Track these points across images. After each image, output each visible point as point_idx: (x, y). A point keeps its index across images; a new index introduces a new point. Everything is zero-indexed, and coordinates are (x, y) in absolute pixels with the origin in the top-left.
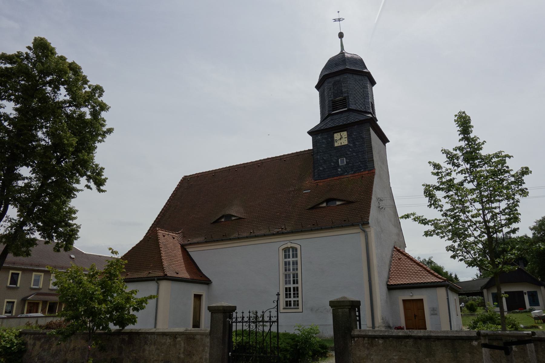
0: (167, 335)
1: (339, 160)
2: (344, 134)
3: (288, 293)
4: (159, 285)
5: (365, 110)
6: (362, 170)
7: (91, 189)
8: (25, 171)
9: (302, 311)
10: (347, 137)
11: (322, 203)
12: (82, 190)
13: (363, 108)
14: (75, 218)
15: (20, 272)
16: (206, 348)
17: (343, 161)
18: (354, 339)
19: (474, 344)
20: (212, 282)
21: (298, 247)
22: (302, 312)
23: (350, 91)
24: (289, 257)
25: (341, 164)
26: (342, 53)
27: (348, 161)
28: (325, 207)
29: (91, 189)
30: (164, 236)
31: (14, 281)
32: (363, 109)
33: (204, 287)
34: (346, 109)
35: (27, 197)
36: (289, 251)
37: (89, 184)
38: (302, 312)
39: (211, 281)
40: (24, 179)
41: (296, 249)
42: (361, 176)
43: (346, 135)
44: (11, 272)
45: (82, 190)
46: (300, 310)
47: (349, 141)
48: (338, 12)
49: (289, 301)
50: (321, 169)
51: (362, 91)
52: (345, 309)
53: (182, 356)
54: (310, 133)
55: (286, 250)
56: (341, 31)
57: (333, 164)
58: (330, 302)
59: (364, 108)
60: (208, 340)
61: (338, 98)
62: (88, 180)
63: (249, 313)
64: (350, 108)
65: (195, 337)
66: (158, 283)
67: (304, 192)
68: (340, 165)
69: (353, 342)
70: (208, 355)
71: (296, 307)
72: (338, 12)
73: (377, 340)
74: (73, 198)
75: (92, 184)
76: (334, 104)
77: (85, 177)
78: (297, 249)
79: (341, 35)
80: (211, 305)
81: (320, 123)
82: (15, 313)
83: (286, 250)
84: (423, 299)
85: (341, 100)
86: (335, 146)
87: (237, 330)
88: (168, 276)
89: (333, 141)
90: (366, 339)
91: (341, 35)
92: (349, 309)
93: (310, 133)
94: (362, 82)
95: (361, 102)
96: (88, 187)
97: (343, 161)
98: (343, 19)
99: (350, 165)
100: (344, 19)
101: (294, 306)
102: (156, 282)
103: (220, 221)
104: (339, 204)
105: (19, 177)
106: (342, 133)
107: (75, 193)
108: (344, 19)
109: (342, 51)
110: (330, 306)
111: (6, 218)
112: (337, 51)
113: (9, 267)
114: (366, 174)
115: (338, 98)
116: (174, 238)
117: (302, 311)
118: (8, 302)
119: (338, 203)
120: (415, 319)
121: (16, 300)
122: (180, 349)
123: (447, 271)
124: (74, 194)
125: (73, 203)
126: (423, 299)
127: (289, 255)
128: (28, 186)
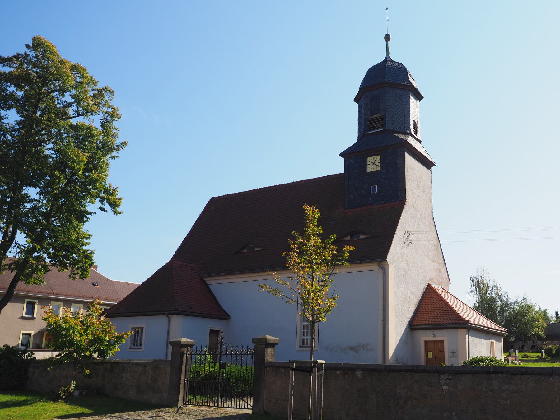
0: (139, 365)
1: (371, 187)
2: (378, 158)
3: (305, 330)
4: (170, 320)
5: (404, 131)
6: (394, 200)
7: (106, 211)
8: (32, 192)
9: (317, 350)
10: (368, 166)
11: (346, 236)
12: (95, 213)
13: (402, 128)
14: (88, 243)
15: (37, 301)
16: (167, 375)
17: (374, 189)
18: (267, 369)
19: (338, 373)
20: (231, 318)
22: (318, 351)
23: (387, 109)
25: (372, 192)
26: (388, 59)
27: (380, 189)
28: (348, 240)
29: (106, 211)
30: (181, 267)
31: (31, 311)
32: (402, 130)
33: (223, 322)
34: (382, 129)
35: (27, 230)
37: (103, 206)
38: (318, 351)
39: (229, 316)
40: (31, 201)
42: (391, 207)
43: (380, 160)
44: (26, 300)
45: (95, 213)
47: (382, 167)
48: (387, 9)
49: (306, 339)
50: (352, 197)
51: (402, 108)
52: (263, 345)
53: (149, 382)
54: (341, 155)
56: (388, 33)
57: (364, 192)
58: (253, 339)
59: (403, 128)
60: (169, 369)
61: (374, 116)
62: (102, 202)
63: (196, 348)
64: (386, 128)
65: (160, 366)
66: (169, 318)
67: (331, 222)
68: (371, 193)
69: (265, 371)
70: (168, 381)
72: (387, 9)
73: (280, 369)
74: (87, 221)
75: (106, 206)
76: (371, 123)
77: (98, 199)
80: (174, 340)
81: (357, 142)
82: (32, 345)
84: (444, 341)
85: (377, 119)
86: (368, 172)
88: (179, 311)
89: (365, 165)
90: (274, 368)
91: (387, 38)
92: (265, 345)
93: (341, 155)
94: (403, 97)
95: (400, 122)
96: (102, 209)
97: (374, 189)
99: (381, 193)
102: (167, 317)
103: (242, 251)
104: (363, 238)
105: (26, 198)
106: (375, 157)
107: (88, 216)
110: (253, 342)
111: (15, 244)
112: (381, 58)
113: (24, 295)
114: (397, 205)
115: (374, 116)
116: (193, 270)
117: (317, 350)
118: (23, 334)
119: (362, 237)
120: (436, 360)
121: (33, 332)
122: (148, 377)
124: (87, 218)
125: (86, 227)
126: (444, 341)
128: (35, 208)
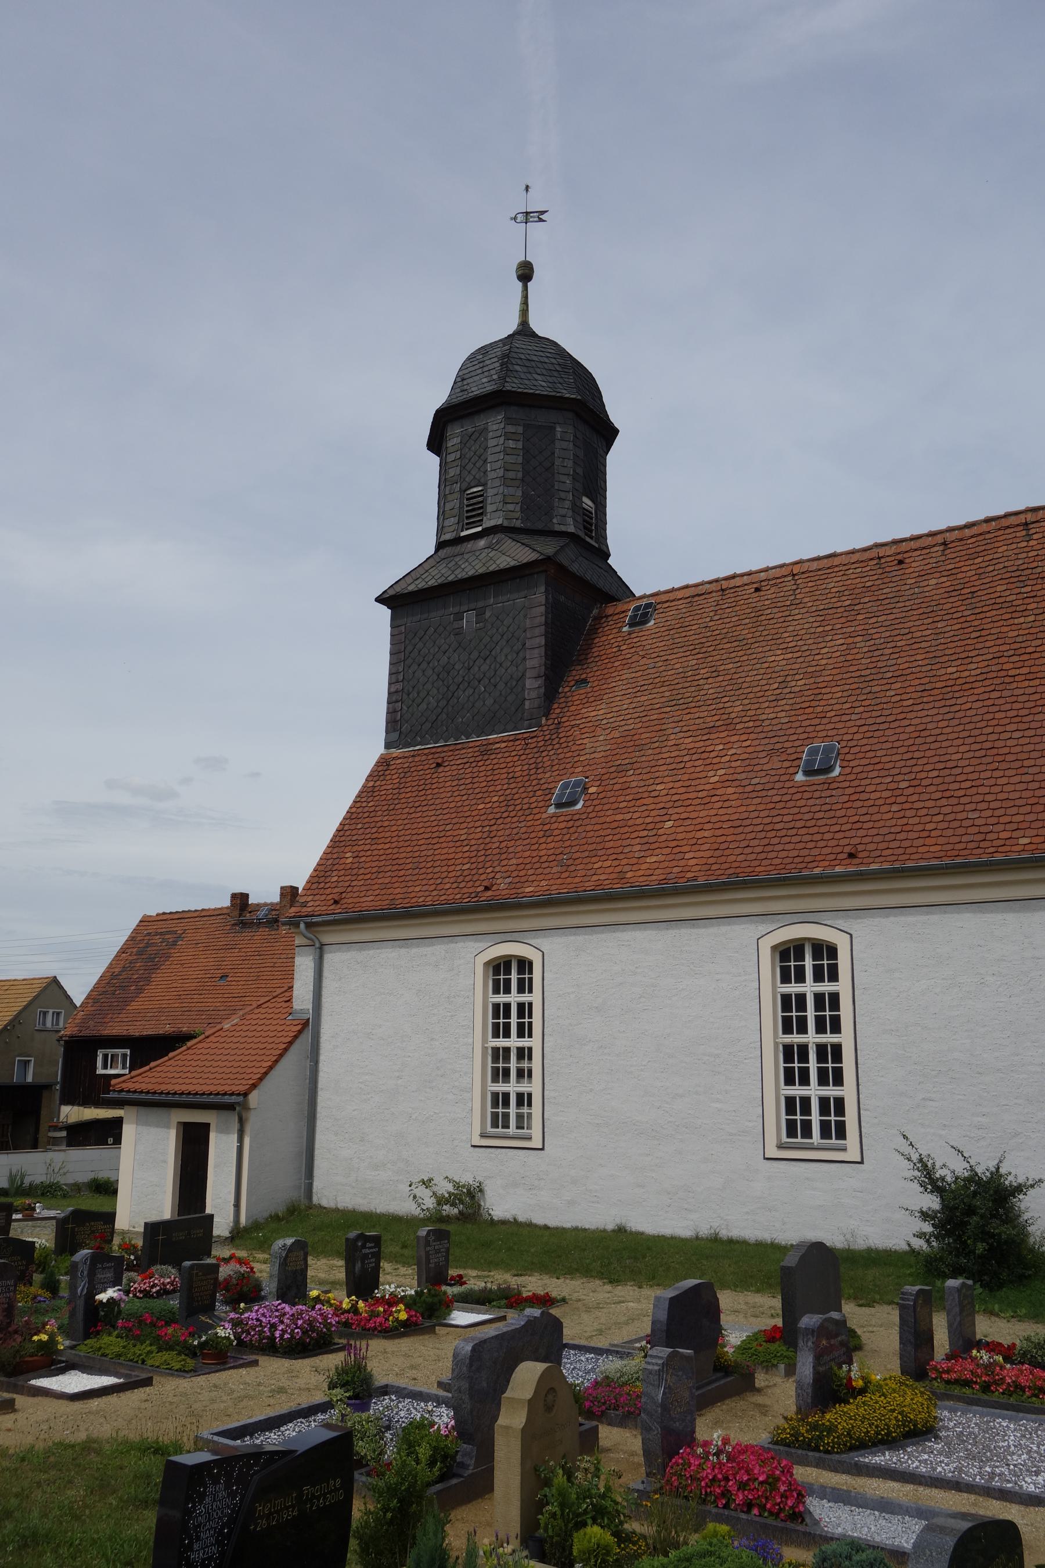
21: (841, 942)
22: (862, 1162)
24: (507, 991)
36: (800, 957)
41: (832, 951)
46: (853, 1155)
55: (500, 967)
71: (500, 1130)
78: (836, 949)
79: (525, 272)
83: (500, 967)
87: (235, 1137)
91: (525, 272)
98: (515, 219)
100: (511, 219)
101: (518, 1128)
108: (511, 219)
109: (524, 323)
117: (541, 1147)
123: (1016, 1171)
127: (508, 982)
